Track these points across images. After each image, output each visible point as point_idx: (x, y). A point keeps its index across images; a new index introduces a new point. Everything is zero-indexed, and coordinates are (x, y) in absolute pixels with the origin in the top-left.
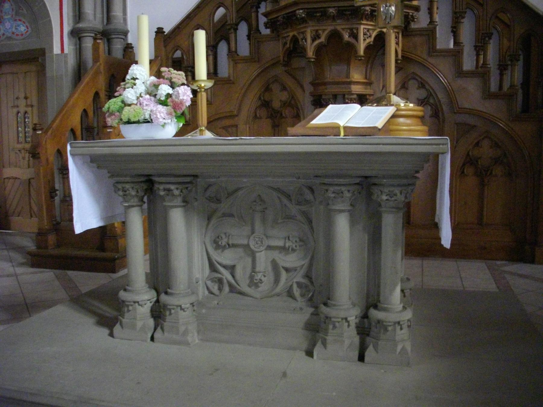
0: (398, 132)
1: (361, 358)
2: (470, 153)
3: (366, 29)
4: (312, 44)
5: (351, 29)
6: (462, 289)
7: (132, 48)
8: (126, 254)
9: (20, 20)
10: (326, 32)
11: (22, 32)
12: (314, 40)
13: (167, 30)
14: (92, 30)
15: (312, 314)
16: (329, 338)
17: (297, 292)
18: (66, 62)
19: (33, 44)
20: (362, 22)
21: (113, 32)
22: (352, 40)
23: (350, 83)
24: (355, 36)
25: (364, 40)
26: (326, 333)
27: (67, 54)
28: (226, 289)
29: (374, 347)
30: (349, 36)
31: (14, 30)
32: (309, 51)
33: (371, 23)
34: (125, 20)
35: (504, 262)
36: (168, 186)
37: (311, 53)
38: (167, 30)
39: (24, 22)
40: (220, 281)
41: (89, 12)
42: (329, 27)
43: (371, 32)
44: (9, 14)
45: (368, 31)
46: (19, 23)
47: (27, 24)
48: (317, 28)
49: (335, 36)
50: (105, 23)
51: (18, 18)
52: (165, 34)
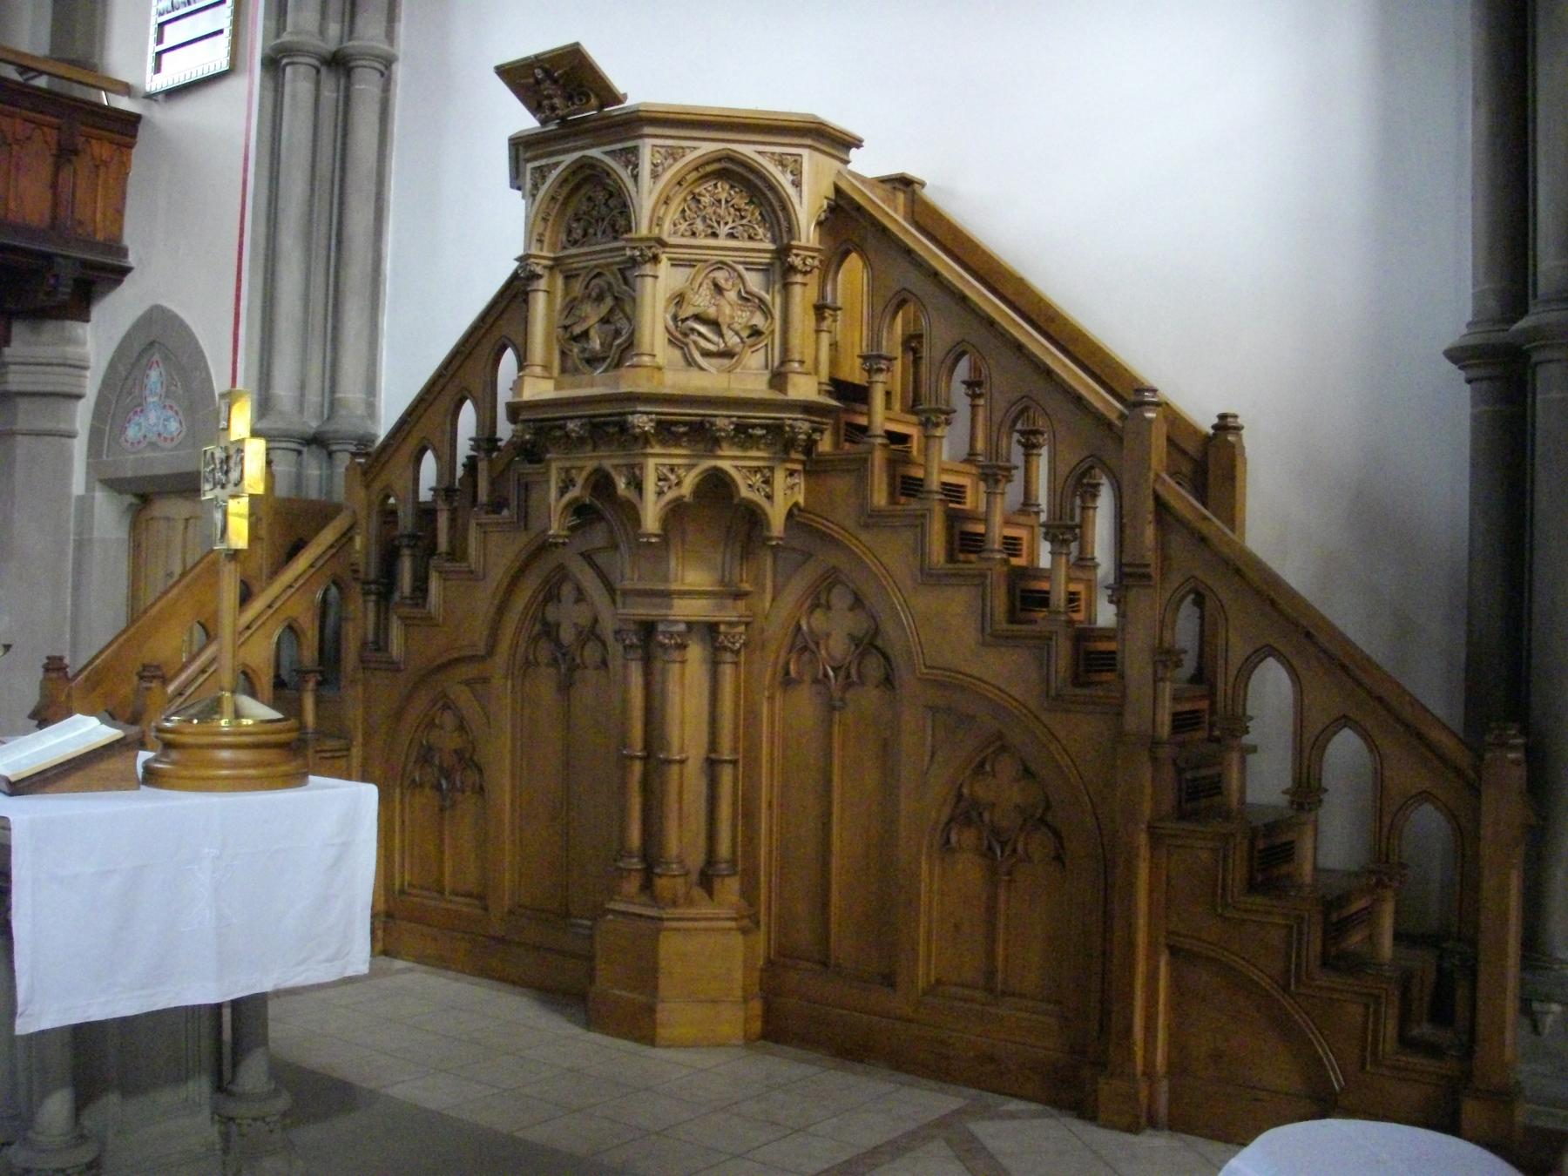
2: (965, 791)
3: (664, 465)
4: (558, 500)
5: (632, 466)
8: (1522, 979)
10: (584, 474)
11: (171, 433)
12: (563, 491)
20: (650, 451)
21: (334, 438)
23: (667, 595)
24: (637, 484)
25: (660, 493)
31: (161, 428)
35: (1033, 1106)
41: (282, 393)
42: (591, 463)
43: (682, 472)
44: (156, 394)
46: (170, 413)
48: (568, 464)
50: (326, 416)
51: (168, 403)
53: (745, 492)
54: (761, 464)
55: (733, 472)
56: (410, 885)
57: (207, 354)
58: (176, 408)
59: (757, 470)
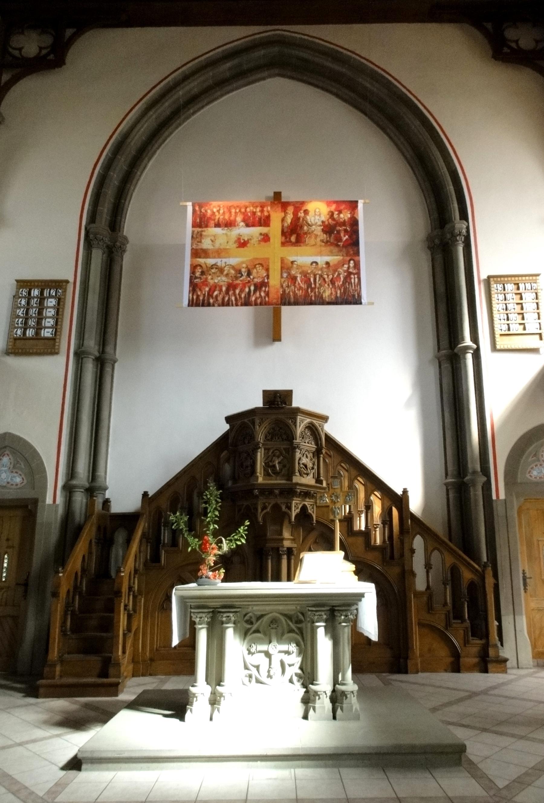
0: (511, 607)
1: (334, 718)
6: (341, 769)
7: (110, 502)
9: (16, 472)
10: (270, 505)
12: (262, 510)
13: (151, 494)
14: (82, 487)
15: (305, 692)
16: (317, 706)
17: (295, 679)
18: (56, 511)
19: (29, 494)
22: (287, 510)
24: (290, 508)
25: (295, 510)
26: (314, 701)
27: (58, 505)
28: (254, 680)
29: (341, 708)
30: (286, 508)
31: (9, 480)
32: (259, 518)
33: (299, 499)
34: (105, 478)
36: (228, 614)
37: (261, 519)
38: (151, 494)
39: (20, 475)
40: (250, 676)
45: (297, 504)
46: (15, 475)
47: (23, 476)
49: (276, 507)
51: (14, 471)
52: (150, 496)
53: (309, 511)
54: (311, 503)
55: (307, 505)
56: (159, 647)
57: (41, 454)
58: (20, 473)
59: (311, 505)
